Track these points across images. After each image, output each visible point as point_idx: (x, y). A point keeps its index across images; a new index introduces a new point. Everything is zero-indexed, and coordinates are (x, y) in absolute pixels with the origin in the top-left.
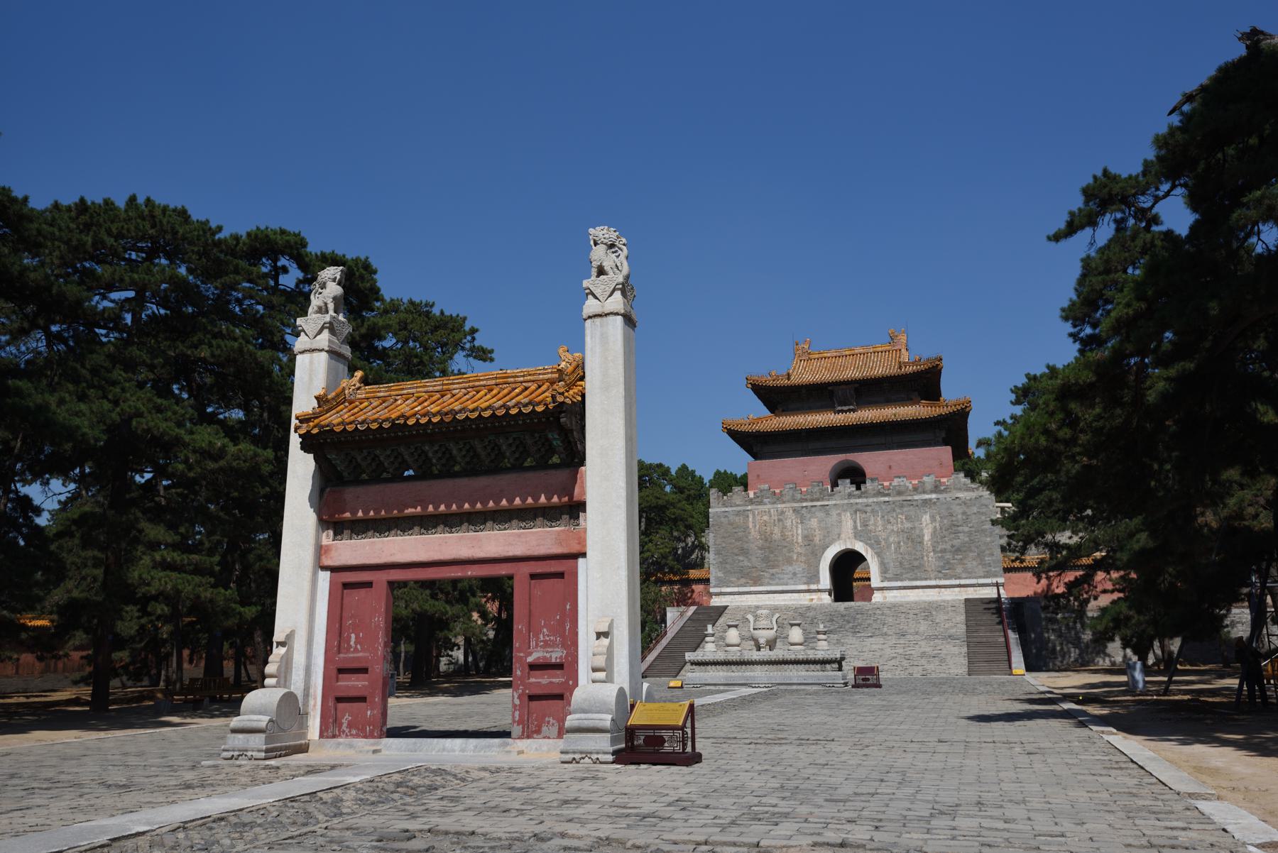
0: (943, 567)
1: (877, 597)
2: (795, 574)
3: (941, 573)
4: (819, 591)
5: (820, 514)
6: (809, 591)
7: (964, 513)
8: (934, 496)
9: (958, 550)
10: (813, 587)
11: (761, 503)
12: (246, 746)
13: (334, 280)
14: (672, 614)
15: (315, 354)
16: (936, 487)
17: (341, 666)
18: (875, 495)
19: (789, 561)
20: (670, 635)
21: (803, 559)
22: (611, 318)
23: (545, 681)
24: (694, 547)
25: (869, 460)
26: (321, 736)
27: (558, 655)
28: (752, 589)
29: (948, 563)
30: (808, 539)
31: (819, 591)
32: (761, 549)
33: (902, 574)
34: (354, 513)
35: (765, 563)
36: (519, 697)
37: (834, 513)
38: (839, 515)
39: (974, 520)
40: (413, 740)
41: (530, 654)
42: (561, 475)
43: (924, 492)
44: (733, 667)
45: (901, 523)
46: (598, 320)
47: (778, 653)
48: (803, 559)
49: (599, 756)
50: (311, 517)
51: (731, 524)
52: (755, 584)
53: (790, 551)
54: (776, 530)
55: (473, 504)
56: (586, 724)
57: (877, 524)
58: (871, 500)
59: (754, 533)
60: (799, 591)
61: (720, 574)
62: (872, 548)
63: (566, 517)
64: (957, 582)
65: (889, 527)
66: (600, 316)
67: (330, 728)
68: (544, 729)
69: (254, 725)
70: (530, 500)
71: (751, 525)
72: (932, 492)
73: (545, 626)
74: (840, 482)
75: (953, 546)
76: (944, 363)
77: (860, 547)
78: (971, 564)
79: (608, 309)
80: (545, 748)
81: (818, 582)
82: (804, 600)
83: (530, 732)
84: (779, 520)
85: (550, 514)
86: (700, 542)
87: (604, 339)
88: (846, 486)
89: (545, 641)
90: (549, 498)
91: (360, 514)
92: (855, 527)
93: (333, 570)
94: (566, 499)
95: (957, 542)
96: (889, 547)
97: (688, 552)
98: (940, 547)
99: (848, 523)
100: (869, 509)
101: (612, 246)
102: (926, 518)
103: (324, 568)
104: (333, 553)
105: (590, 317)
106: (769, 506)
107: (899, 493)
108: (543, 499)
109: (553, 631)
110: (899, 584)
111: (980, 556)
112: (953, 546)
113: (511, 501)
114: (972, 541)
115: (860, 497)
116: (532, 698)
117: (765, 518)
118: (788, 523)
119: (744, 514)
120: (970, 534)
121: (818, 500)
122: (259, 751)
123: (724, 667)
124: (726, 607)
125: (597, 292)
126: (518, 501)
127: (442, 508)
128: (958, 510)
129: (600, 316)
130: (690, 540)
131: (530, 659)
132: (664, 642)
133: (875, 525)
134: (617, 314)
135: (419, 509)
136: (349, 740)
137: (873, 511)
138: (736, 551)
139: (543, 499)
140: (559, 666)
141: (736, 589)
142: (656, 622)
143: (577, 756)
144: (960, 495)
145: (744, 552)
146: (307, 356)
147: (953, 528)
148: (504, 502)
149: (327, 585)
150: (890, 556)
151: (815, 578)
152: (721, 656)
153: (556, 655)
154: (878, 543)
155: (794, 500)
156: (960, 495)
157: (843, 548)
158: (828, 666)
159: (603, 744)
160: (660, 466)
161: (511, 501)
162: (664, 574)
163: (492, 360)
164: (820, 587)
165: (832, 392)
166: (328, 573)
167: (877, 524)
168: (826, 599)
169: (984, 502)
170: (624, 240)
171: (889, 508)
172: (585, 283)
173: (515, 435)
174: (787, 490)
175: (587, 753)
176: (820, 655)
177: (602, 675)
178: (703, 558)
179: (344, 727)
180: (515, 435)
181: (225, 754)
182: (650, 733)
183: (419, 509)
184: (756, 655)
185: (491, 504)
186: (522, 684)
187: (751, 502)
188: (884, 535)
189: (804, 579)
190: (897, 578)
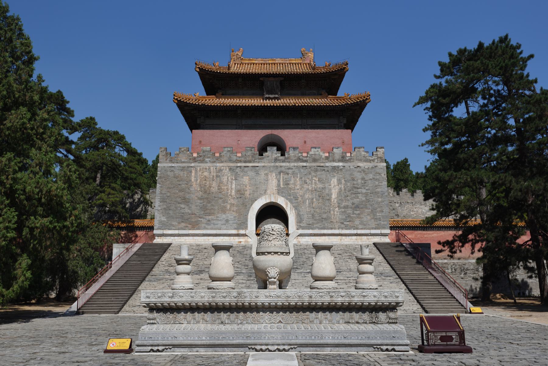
0: (345, 220)
2: (227, 221)
3: (343, 224)
5: (251, 173)
7: (363, 179)
8: (341, 164)
9: (357, 207)
10: (242, 232)
11: (203, 161)
14: (117, 249)
16: (343, 157)
18: (295, 161)
19: (224, 210)
20: (115, 268)
21: (235, 208)
24: (140, 202)
25: (291, 136)
28: (191, 232)
29: (349, 216)
30: (240, 193)
32: (200, 199)
33: (313, 224)
35: (204, 209)
37: (262, 173)
38: (266, 175)
39: (370, 184)
43: (334, 161)
44: (223, 316)
45: (314, 183)
47: (295, 293)
48: (235, 208)
51: (175, 177)
52: (193, 228)
53: (225, 202)
54: (214, 184)
57: (296, 183)
58: (292, 164)
59: (195, 186)
60: (230, 235)
61: (164, 219)
62: (291, 203)
64: (355, 232)
65: (306, 186)
71: (193, 179)
72: (339, 161)
74: (268, 148)
75: (353, 204)
76: (349, 67)
77: (281, 201)
78: (366, 218)
81: (246, 228)
84: (217, 176)
86: (145, 199)
88: (272, 152)
92: (279, 185)
95: (356, 201)
96: (304, 202)
97: (134, 206)
98: (344, 204)
99: (273, 182)
100: (290, 171)
102: (334, 181)
106: (209, 164)
107: (315, 160)
110: (311, 231)
111: (373, 212)
112: (353, 204)
114: (368, 201)
115: (283, 161)
117: (206, 174)
118: (225, 179)
119: (188, 170)
120: (366, 194)
121: (250, 162)
123: (208, 316)
124: (170, 245)
128: (358, 176)
130: (137, 197)
132: (108, 275)
133: (295, 184)
137: (293, 173)
138: (179, 200)
141: (176, 232)
142: (104, 259)
144: (360, 164)
145: (186, 201)
147: (354, 190)
150: (305, 209)
151: (243, 224)
152: (203, 297)
154: (296, 198)
155: (230, 161)
156: (360, 164)
157: (268, 201)
158: (382, 316)
160: (116, 133)
162: (114, 222)
165: (262, 83)
167: (296, 183)
169: (378, 171)
171: (306, 171)
174: (225, 154)
178: (146, 211)
184: (263, 297)
187: (195, 160)
188: (301, 192)
189: (235, 226)
190: (309, 227)
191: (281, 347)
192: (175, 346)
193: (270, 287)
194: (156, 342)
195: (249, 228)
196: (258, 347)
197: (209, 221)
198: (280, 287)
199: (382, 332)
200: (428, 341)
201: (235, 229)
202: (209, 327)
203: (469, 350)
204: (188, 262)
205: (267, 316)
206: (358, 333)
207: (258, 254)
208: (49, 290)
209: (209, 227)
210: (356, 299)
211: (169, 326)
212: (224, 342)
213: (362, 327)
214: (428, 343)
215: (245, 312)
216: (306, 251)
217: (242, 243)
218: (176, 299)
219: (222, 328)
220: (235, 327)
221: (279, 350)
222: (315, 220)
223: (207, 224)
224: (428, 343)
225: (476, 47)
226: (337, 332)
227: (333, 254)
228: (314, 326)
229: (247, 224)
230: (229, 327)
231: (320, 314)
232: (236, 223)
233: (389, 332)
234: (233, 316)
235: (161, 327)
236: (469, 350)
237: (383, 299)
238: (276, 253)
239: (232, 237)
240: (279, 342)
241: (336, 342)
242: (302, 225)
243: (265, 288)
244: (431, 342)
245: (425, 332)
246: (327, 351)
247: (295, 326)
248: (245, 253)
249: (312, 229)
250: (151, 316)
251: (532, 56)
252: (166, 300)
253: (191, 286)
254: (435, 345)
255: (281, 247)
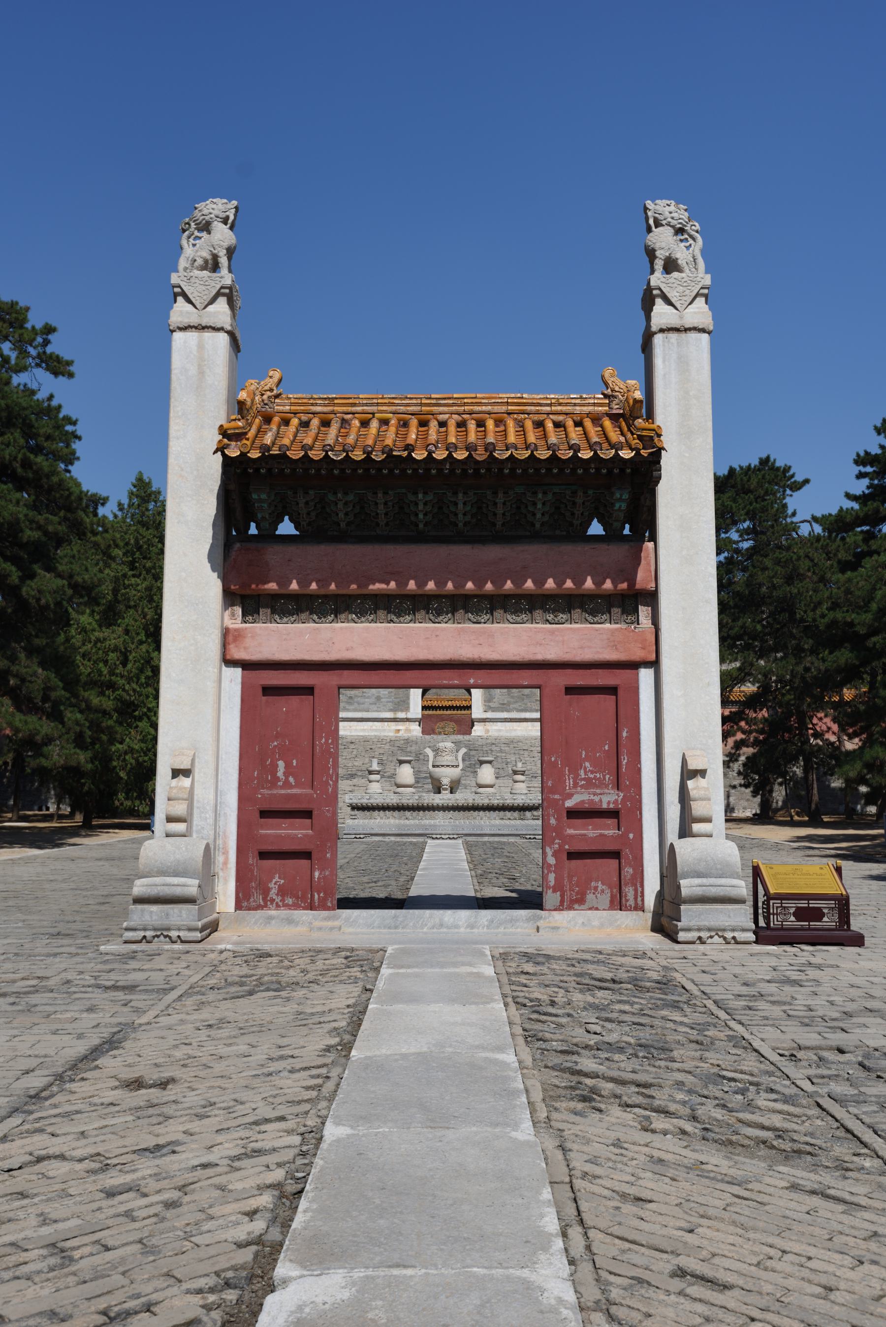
1: (478, 730)
4: (408, 720)
6: (395, 720)
12: (166, 923)
13: (225, 221)
15: (207, 335)
17: (266, 807)
22: (693, 335)
23: (591, 833)
26: (238, 906)
27: (613, 798)
31: (408, 720)
33: (509, 703)
34: (284, 582)
36: (555, 854)
40: (393, 912)
41: (570, 796)
42: (617, 552)
44: (408, 814)
46: (673, 336)
47: (462, 797)
49: (736, 934)
50: (212, 586)
55: (480, 583)
56: (713, 892)
63: (616, 611)
66: (677, 330)
67: (244, 899)
68: (590, 897)
69: (178, 891)
70: (569, 584)
73: (587, 758)
79: (689, 322)
80: (596, 923)
81: (407, 709)
82: (388, 730)
83: (574, 900)
85: (593, 606)
87: (683, 363)
89: (588, 780)
90: (598, 583)
91: (294, 586)
93: (247, 666)
94: (624, 586)
101: (680, 231)
103: (229, 662)
104: (248, 642)
105: (662, 331)
108: (589, 584)
109: (598, 766)
110: (505, 715)
113: (540, 583)
116: (572, 855)
122: (190, 929)
123: (396, 813)
125: (672, 295)
126: (550, 584)
127: (431, 585)
129: (677, 330)
131: (569, 804)
134: (703, 331)
135: (393, 584)
136: (283, 913)
139: (589, 584)
140: (613, 814)
143: (149, 934)
146: (192, 335)
148: (529, 584)
149: (238, 688)
153: (608, 799)
159: (740, 917)
161: (540, 583)
163: (71, 375)
164: (410, 716)
166: (238, 671)
168: (416, 730)
170: (698, 227)
172: (174, 279)
173: (556, 490)
175: (718, 931)
176: (520, 800)
177: (180, 827)
179: (273, 893)
180: (556, 490)
181: (129, 935)
182: (803, 904)
183: (393, 584)
185: (509, 585)
186: (559, 836)
191: (451, 836)
192: (372, 835)
193: (443, 792)
194: (358, 832)
195: (411, 709)
196: (434, 836)
197: (351, 698)
198: (451, 793)
199: (528, 825)
200: (767, 919)
201: (391, 710)
202: (397, 821)
203: (858, 941)
204: (378, 772)
205: (441, 813)
206: (508, 826)
207: (434, 766)
208: (790, 762)
209: (351, 707)
210: (508, 802)
211: (367, 821)
212: (409, 832)
213: (512, 822)
214: (768, 923)
215: (424, 811)
216: (494, 748)
217: (401, 733)
218: (372, 801)
219: (407, 822)
220: (417, 822)
221: (450, 838)
222: (513, 697)
223: (348, 703)
224: (768, 923)
225: (726, 473)
226: (493, 826)
227: (493, 766)
228: (477, 821)
229: (408, 704)
230: (412, 822)
231: (481, 813)
232: (392, 702)
233: (532, 826)
234: (415, 813)
235: (361, 821)
236: (858, 941)
237: (529, 801)
238: (448, 766)
239: (386, 723)
240: (450, 832)
241: (493, 832)
242: (492, 705)
243: (440, 793)
244: (775, 922)
245: (761, 899)
246: (486, 839)
247: (462, 821)
248: (409, 749)
249: (508, 711)
250: (353, 813)
251: (807, 481)
252: (364, 801)
253: (381, 791)
254: (782, 929)
255: (452, 761)
